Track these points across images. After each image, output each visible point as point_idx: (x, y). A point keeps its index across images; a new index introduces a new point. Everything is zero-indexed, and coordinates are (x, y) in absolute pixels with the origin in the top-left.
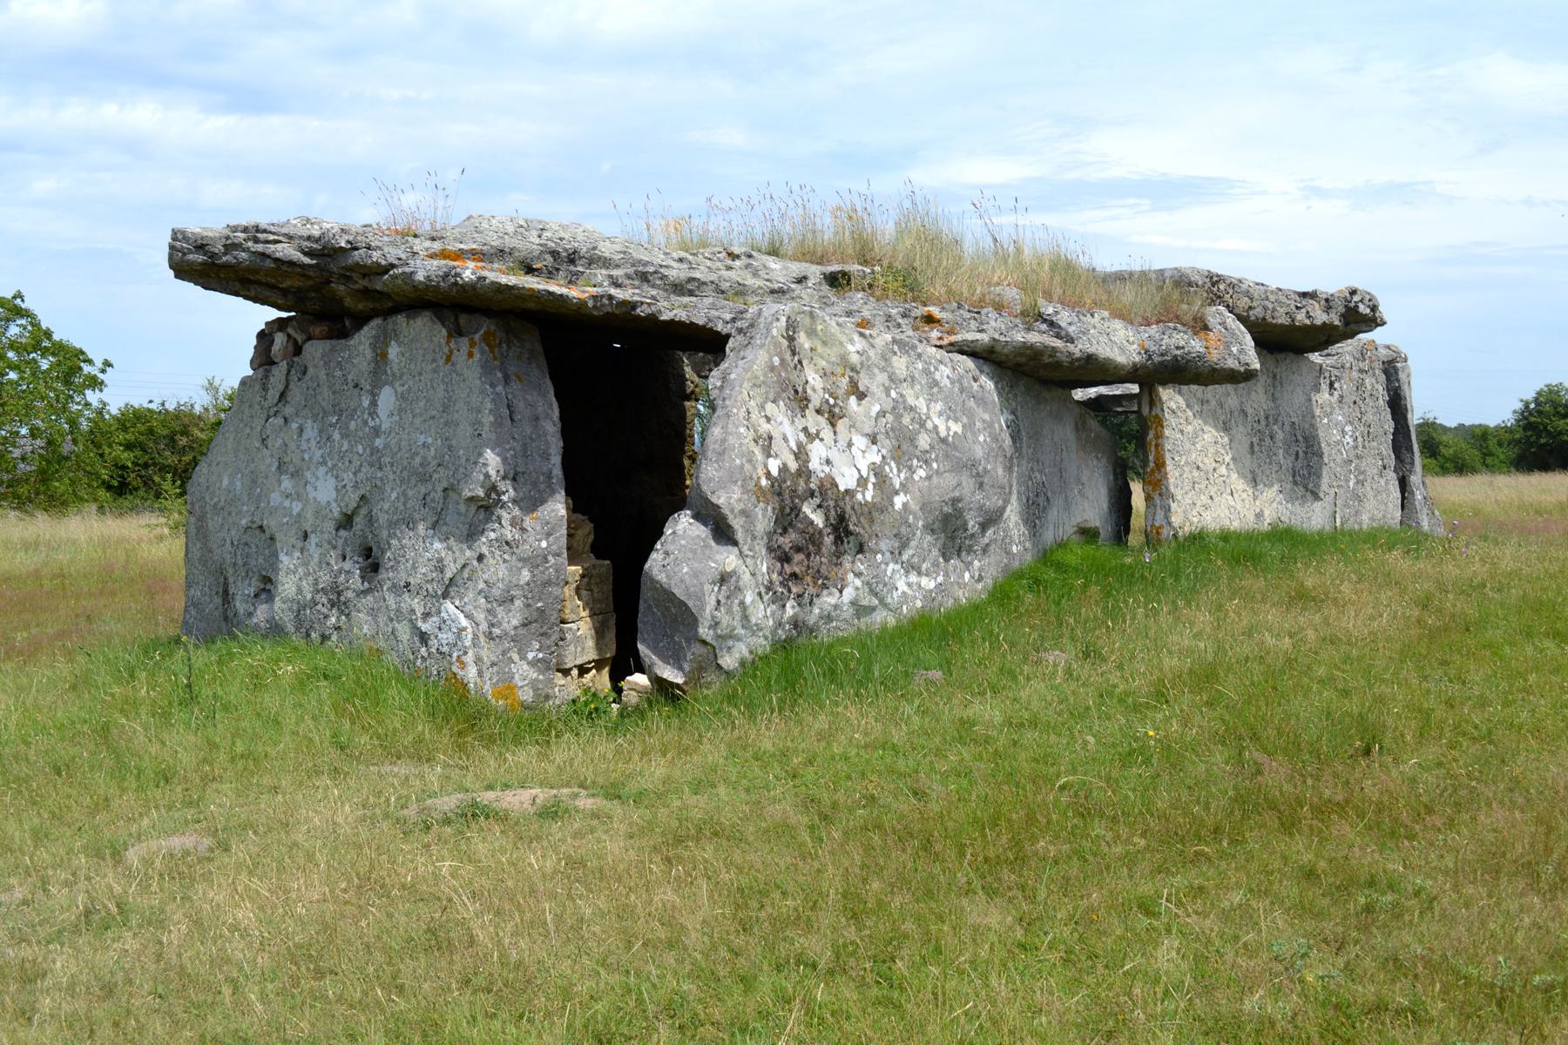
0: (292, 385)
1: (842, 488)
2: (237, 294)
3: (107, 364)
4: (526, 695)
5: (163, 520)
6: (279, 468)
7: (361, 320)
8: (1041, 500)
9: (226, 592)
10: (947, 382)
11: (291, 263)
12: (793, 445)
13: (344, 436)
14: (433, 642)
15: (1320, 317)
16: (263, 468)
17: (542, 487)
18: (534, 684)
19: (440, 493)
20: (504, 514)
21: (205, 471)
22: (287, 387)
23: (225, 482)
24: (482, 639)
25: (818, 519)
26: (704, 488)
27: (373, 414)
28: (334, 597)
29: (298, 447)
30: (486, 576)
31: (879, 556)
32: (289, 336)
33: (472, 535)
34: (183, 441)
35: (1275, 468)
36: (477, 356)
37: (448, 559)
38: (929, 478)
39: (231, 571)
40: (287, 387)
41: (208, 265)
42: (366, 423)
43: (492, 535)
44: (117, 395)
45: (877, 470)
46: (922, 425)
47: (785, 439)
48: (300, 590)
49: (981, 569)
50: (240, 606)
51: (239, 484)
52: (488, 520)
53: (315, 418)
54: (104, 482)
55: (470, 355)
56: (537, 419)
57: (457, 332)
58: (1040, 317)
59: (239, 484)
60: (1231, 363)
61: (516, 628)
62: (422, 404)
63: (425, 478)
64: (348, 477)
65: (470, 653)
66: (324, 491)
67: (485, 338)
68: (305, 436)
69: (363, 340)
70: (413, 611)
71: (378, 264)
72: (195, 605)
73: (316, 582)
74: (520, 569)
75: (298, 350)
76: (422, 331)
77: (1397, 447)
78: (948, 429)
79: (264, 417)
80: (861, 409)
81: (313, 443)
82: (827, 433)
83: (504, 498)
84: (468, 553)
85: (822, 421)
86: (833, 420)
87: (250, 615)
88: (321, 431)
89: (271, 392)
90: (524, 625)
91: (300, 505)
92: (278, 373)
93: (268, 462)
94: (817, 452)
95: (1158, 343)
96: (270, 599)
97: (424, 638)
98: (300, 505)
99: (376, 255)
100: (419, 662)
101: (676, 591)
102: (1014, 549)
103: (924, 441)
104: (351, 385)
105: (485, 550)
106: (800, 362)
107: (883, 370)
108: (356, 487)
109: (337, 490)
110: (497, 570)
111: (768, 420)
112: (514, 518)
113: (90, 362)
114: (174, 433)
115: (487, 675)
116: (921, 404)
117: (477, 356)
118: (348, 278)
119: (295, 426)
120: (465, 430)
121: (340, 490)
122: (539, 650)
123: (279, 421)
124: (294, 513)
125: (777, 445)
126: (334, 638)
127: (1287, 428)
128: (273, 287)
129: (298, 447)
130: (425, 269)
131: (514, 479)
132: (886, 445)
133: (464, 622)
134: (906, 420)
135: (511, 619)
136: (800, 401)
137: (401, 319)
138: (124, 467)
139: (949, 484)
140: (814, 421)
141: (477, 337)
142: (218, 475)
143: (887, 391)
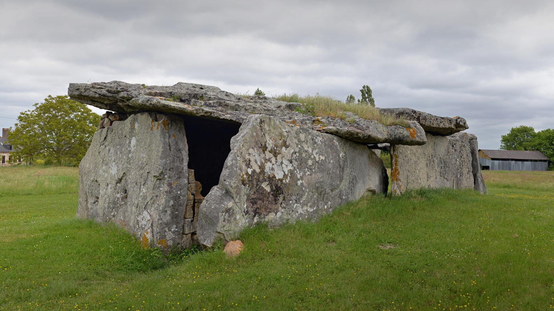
1: (277, 178)
2: (97, 107)
4: (170, 243)
8: (354, 181)
10: (319, 142)
11: (104, 95)
12: (259, 163)
13: (121, 153)
15: (447, 125)
18: (173, 239)
25: (268, 189)
27: (129, 146)
31: (291, 202)
35: (434, 171)
36: (160, 128)
38: (311, 175)
42: (127, 149)
45: (291, 172)
46: (310, 157)
47: (256, 161)
49: (331, 204)
55: (158, 128)
60: (418, 139)
64: (121, 166)
75: (111, 123)
76: (144, 118)
77: (473, 165)
78: (319, 158)
80: (286, 152)
82: (273, 160)
85: (271, 155)
86: (275, 155)
94: (268, 165)
95: (394, 131)
102: (344, 197)
103: (310, 162)
106: (264, 134)
107: (295, 138)
111: (249, 154)
116: (310, 150)
118: (123, 101)
119: (107, 148)
122: (176, 228)
123: (103, 147)
125: (253, 163)
127: (439, 159)
128: (102, 103)
130: (142, 99)
132: (295, 164)
134: (304, 155)
136: (264, 148)
137: (139, 115)
139: (318, 176)
140: (268, 155)
141: (160, 122)
143: (297, 145)
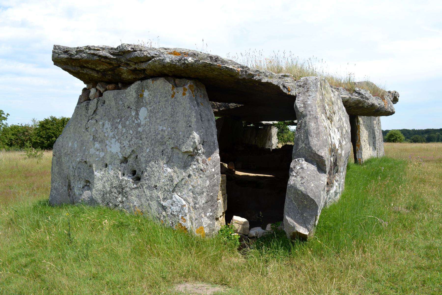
0: (99, 108)
3: (8, 114)
4: (206, 231)
5: (25, 154)
6: (93, 139)
7: (127, 84)
9: (69, 186)
11: (106, 57)
13: (124, 127)
14: (169, 211)
16: (86, 139)
17: (212, 147)
18: (209, 226)
19: (170, 150)
20: (199, 158)
21: (61, 140)
22: (97, 108)
23: (70, 144)
24: (192, 209)
26: (314, 149)
28: (120, 190)
29: (102, 131)
30: (193, 184)
32: (97, 90)
33: (185, 166)
34: (26, 133)
36: (187, 94)
37: (175, 176)
39: (72, 178)
40: (97, 108)
41: (69, 60)
42: (134, 122)
43: (194, 167)
44: (10, 122)
48: (104, 187)
50: (77, 192)
51: (76, 145)
52: (192, 160)
53: (109, 120)
54: (6, 143)
55: (184, 94)
56: (209, 120)
57: (175, 86)
58: (355, 92)
59: (76, 145)
61: (203, 204)
62: (160, 114)
63: (163, 143)
64: (126, 143)
65: (188, 215)
66: (115, 148)
67: (190, 86)
68: (105, 127)
69: (132, 89)
70: (159, 197)
71: (147, 56)
72: (55, 189)
73: (112, 184)
74: (206, 180)
75: (101, 95)
76: (161, 85)
79: (87, 120)
81: (109, 130)
83: (200, 152)
84: (184, 174)
87: (81, 195)
88: (112, 125)
89: (90, 111)
90: (206, 202)
91: (103, 154)
92: (93, 104)
93: (89, 137)
96: (90, 189)
97: (164, 208)
98: (103, 154)
99: (145, 53)
100: (162, 218)
101: (309, 195)
104: (126, 107)
105: (191, 173)
108: (130, 146)
109: (121, 148)
110: (198, 181)
112: (203, 160)
113: (4, 114)
114: (24, 132)
115: (194, 224)
117: (187, 94)
118: (128, 65)
120: (182, 125)
121: (122, 148)
122: (211, 212)
124: (101, 156)
126: (120, 206)
129: (102, 131)
131: (203, 144)
133: (184, 203)
135: (202, 200)
137: (150, 81)
138: (12, 140)
142: (65, 141)
